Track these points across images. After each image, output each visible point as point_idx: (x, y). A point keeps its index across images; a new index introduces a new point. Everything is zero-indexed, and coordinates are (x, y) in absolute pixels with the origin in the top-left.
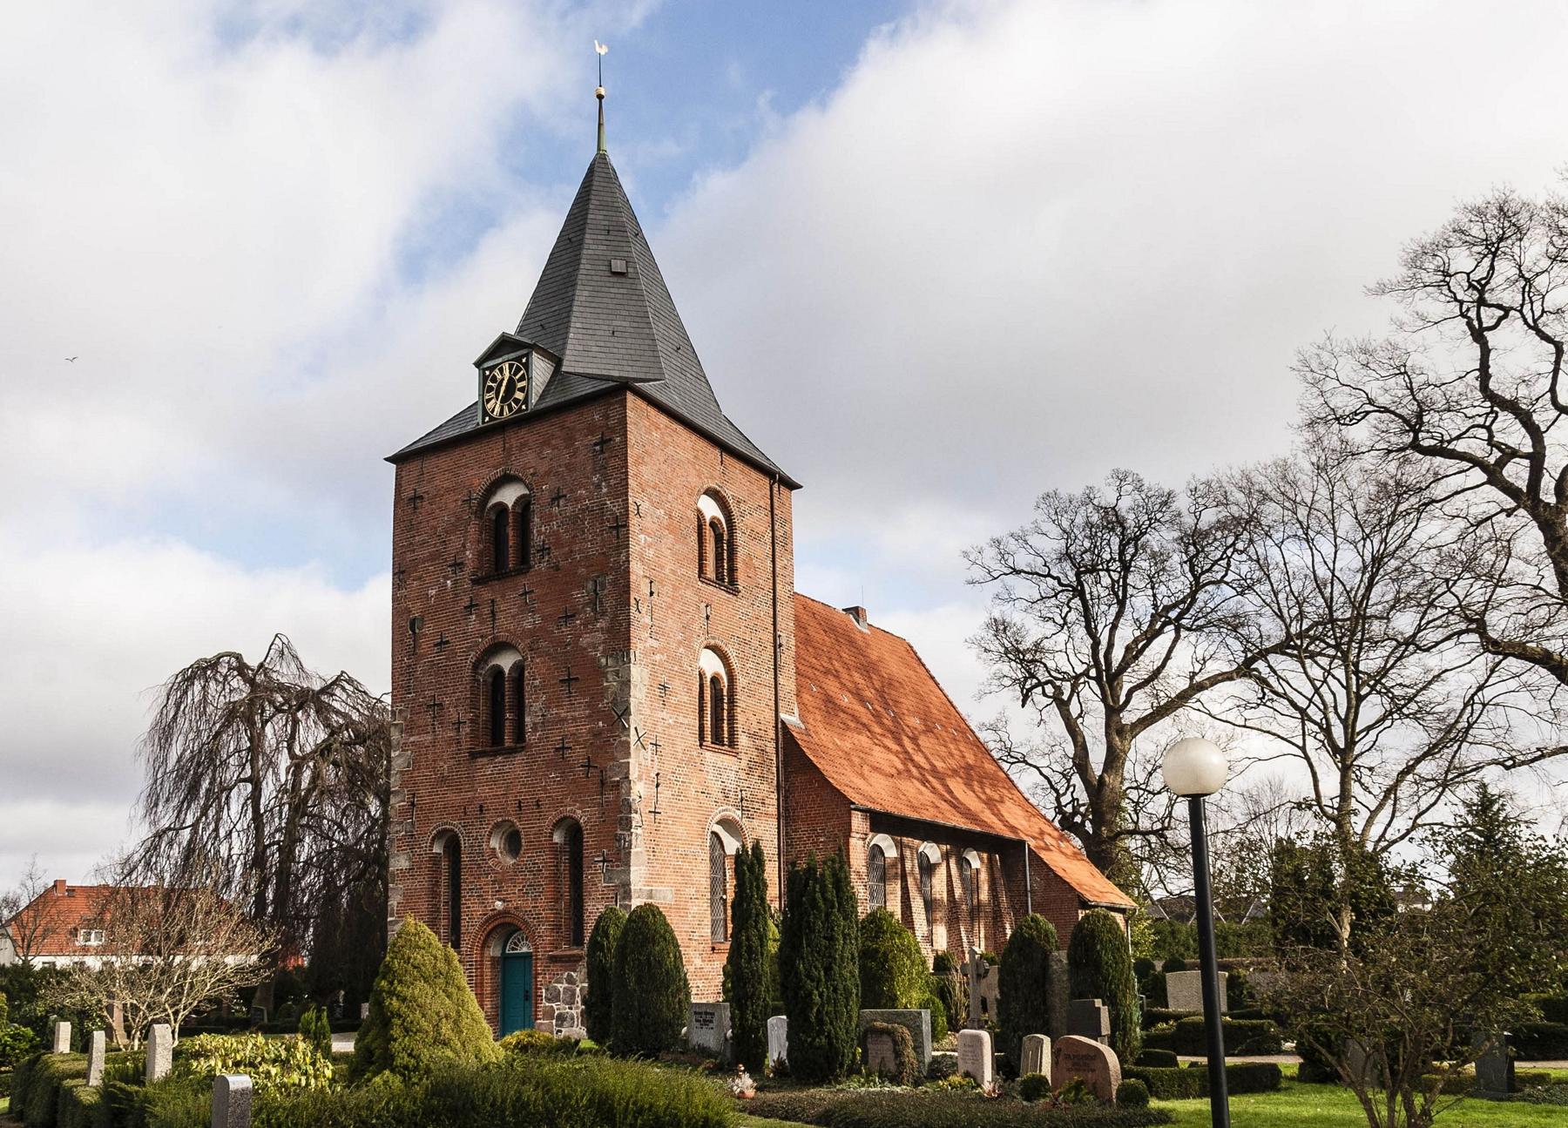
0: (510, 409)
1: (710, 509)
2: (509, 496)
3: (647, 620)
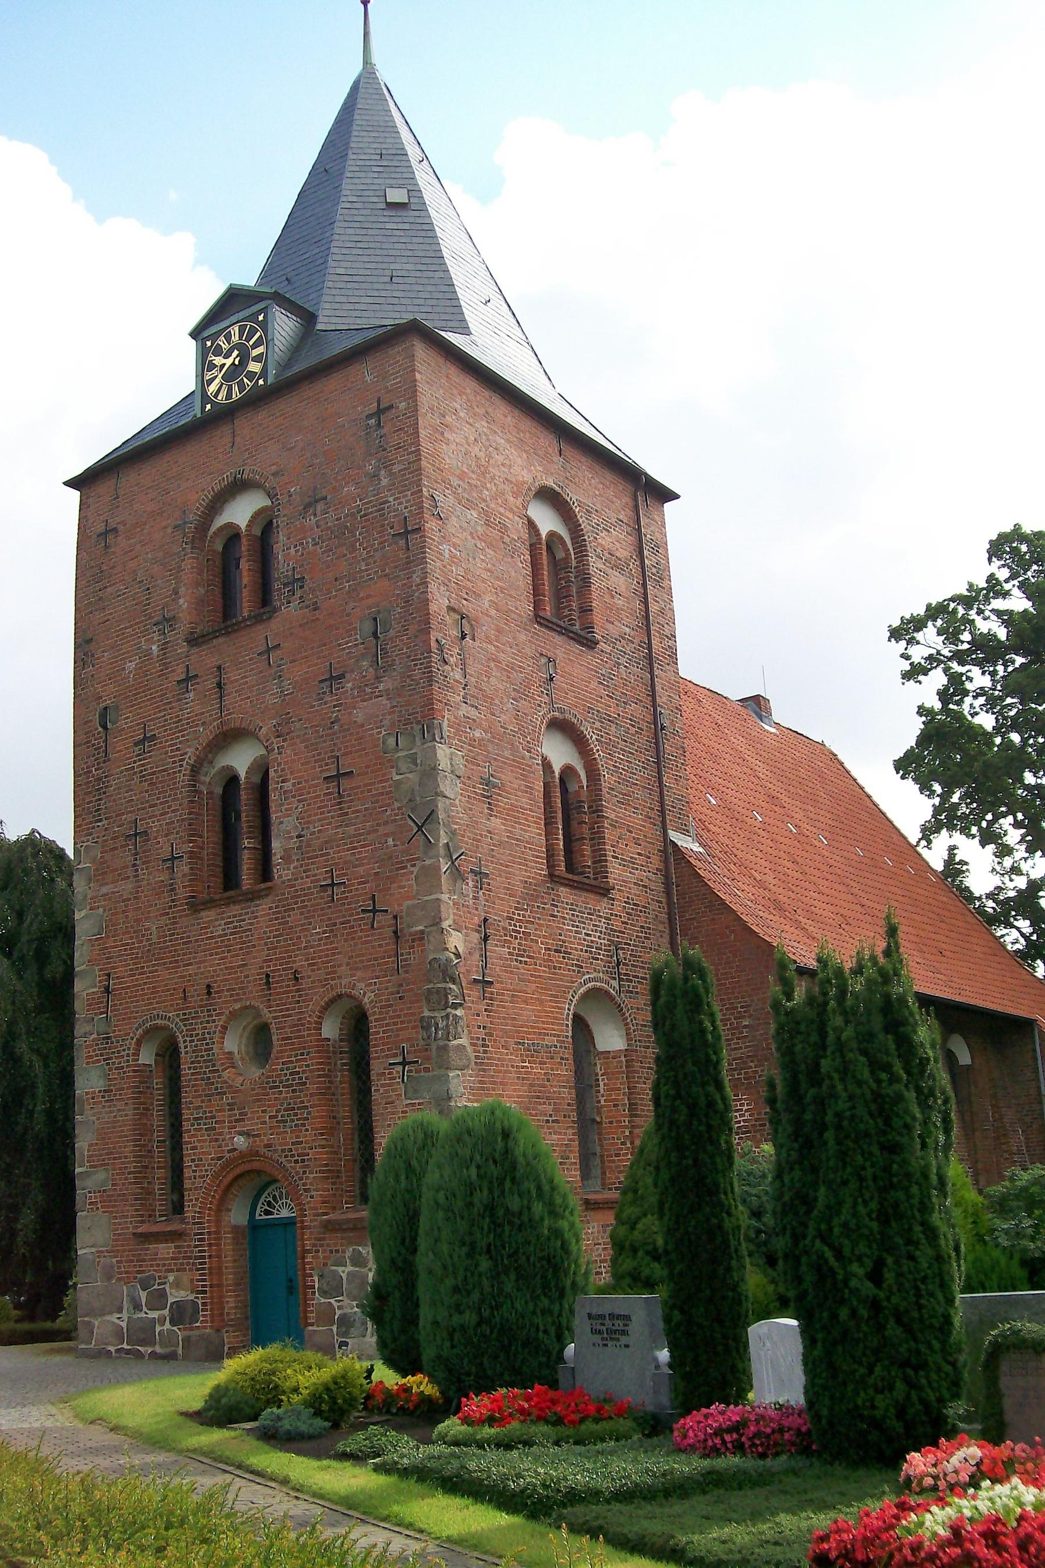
0: (242, 387)
1: (547, 522)
2: (240, 513)
3: (457, 675)
